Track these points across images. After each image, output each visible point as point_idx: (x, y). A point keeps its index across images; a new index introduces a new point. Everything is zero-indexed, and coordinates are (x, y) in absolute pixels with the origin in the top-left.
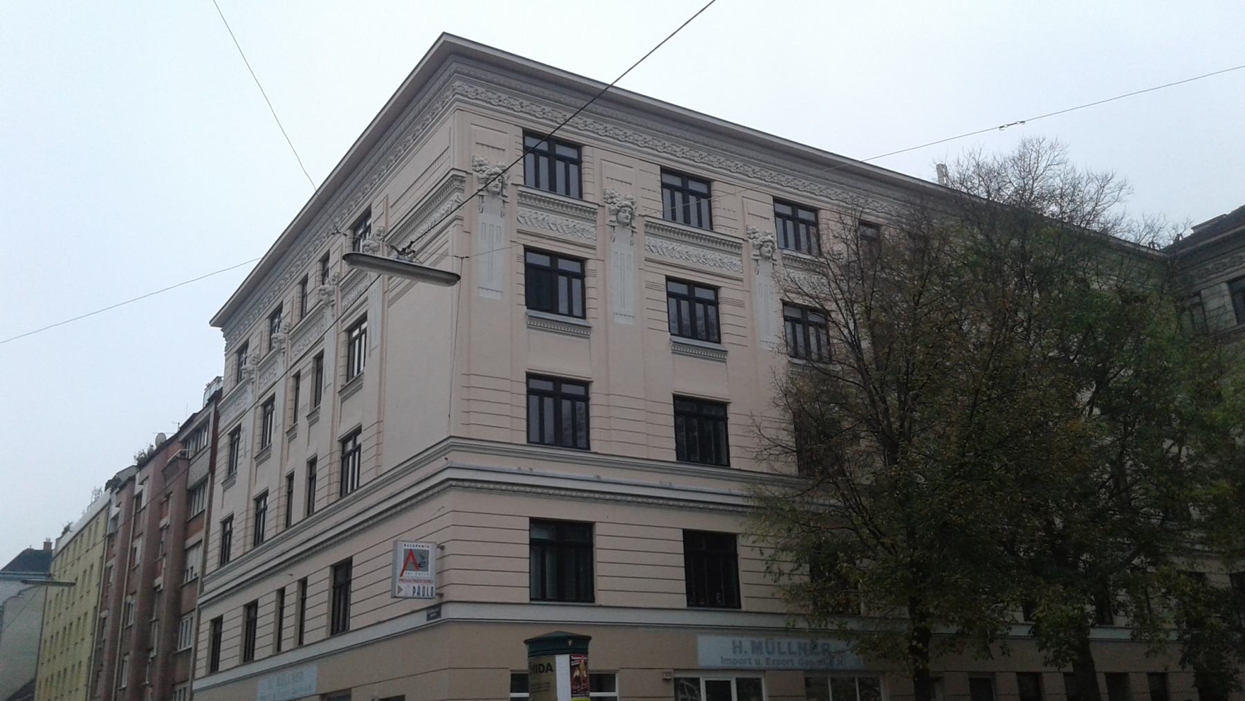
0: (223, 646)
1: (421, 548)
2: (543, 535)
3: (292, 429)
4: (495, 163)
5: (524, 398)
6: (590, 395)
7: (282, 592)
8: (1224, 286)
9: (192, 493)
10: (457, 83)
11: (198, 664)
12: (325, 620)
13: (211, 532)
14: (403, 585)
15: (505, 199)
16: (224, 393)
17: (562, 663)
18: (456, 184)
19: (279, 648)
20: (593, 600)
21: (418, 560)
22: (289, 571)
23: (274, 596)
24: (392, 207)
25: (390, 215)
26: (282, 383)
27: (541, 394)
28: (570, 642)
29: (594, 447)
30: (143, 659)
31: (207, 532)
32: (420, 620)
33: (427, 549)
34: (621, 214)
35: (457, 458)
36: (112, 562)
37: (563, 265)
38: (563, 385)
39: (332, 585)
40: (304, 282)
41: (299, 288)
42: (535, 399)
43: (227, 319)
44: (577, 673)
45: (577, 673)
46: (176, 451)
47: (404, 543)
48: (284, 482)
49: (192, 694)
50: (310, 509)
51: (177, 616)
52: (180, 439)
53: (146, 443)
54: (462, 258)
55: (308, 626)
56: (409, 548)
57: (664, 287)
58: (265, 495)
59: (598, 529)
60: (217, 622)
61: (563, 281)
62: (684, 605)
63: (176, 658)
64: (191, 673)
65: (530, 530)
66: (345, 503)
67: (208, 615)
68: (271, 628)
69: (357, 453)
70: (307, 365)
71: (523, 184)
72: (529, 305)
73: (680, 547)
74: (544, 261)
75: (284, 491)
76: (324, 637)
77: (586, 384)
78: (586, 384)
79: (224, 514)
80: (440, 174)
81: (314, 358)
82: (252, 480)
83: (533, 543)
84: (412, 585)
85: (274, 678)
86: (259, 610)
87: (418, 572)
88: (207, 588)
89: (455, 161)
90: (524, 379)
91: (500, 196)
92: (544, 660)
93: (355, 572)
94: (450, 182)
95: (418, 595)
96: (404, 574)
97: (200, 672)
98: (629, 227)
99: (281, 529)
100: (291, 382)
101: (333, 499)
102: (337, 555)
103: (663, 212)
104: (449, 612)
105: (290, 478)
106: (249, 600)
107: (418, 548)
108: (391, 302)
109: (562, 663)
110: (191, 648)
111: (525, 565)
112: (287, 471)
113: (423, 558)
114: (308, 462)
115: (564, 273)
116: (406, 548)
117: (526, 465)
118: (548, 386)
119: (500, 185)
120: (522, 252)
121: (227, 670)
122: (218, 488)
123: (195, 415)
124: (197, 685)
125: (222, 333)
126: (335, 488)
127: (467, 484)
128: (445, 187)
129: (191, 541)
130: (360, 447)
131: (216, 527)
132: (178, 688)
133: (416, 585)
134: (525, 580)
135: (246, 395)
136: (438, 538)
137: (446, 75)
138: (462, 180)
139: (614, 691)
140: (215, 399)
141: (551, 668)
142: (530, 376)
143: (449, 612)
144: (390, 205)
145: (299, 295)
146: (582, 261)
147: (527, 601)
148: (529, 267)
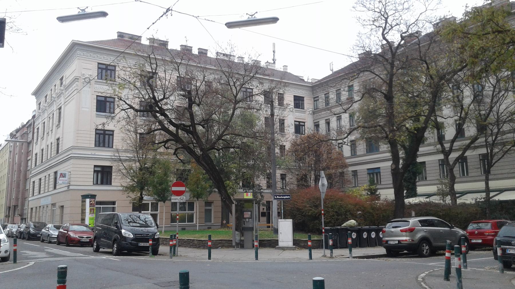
3: (43, 137)
4: (87, 73)
5: (94, 136)
7: (40, 179)
8: (323, 95)
9: (29, 143)
10: (78, 52)
14: (59, 181)
16: (36, 115)
17: (88, 201)
18: (76, 80)
19: (40, 193)
20: (111, 184)
21: (63, 175)
23: (38, 180)
26: (46, 119)
30: (18, 192)
31: (32, 157)
32: (66, 189)
35: (74, 151)
36: (11, 160)
42: (97, 136)
43: (37, 93)
44: (91, 203)
45: (91, 203)
46: (25, 130)
48: (41, 151)
49: (29, 201)
50: (36, 165)
51: (26, 179)
52: (27, 126)
53: (18, 126)
55: (35, 189)
60: (34, 182)
61: (108, 104)
63: (25, 190)
67: (32, 180)
70: (51, 116)
72: (97, 111)
75: (41, 153)
78: (113, 131)
80: (73, 77)
82: (41, 145)
85: (43, 199)
88: (32, 172)
89: (76, 74)
92: (84, 200)
94: (74, 80)
95: (63, 183)
97: (30, 196)
99: (46, 160)
100: (43, 124)
101: (55, 155)
102: (54, 170)
104: (71, 187)
108: (66, 105)
109: (88, 201)
112: (42, 148)
115: (108, 102)
117: (93, 152)
120: (96, 97)
122: (34, 144)
123: (29, 120)
124: (30, 199)
126: (56, 152)
128: (73, 81)
129: (29, 158)
131: (34, 155)
132: (26, 199)
135: (61, 98)
136: (69, 170)
137: (75, 49)
138: (78, 79)
139: (149, 204)
140: (34, 117)
141: (85, 202)
143: (71, 187)
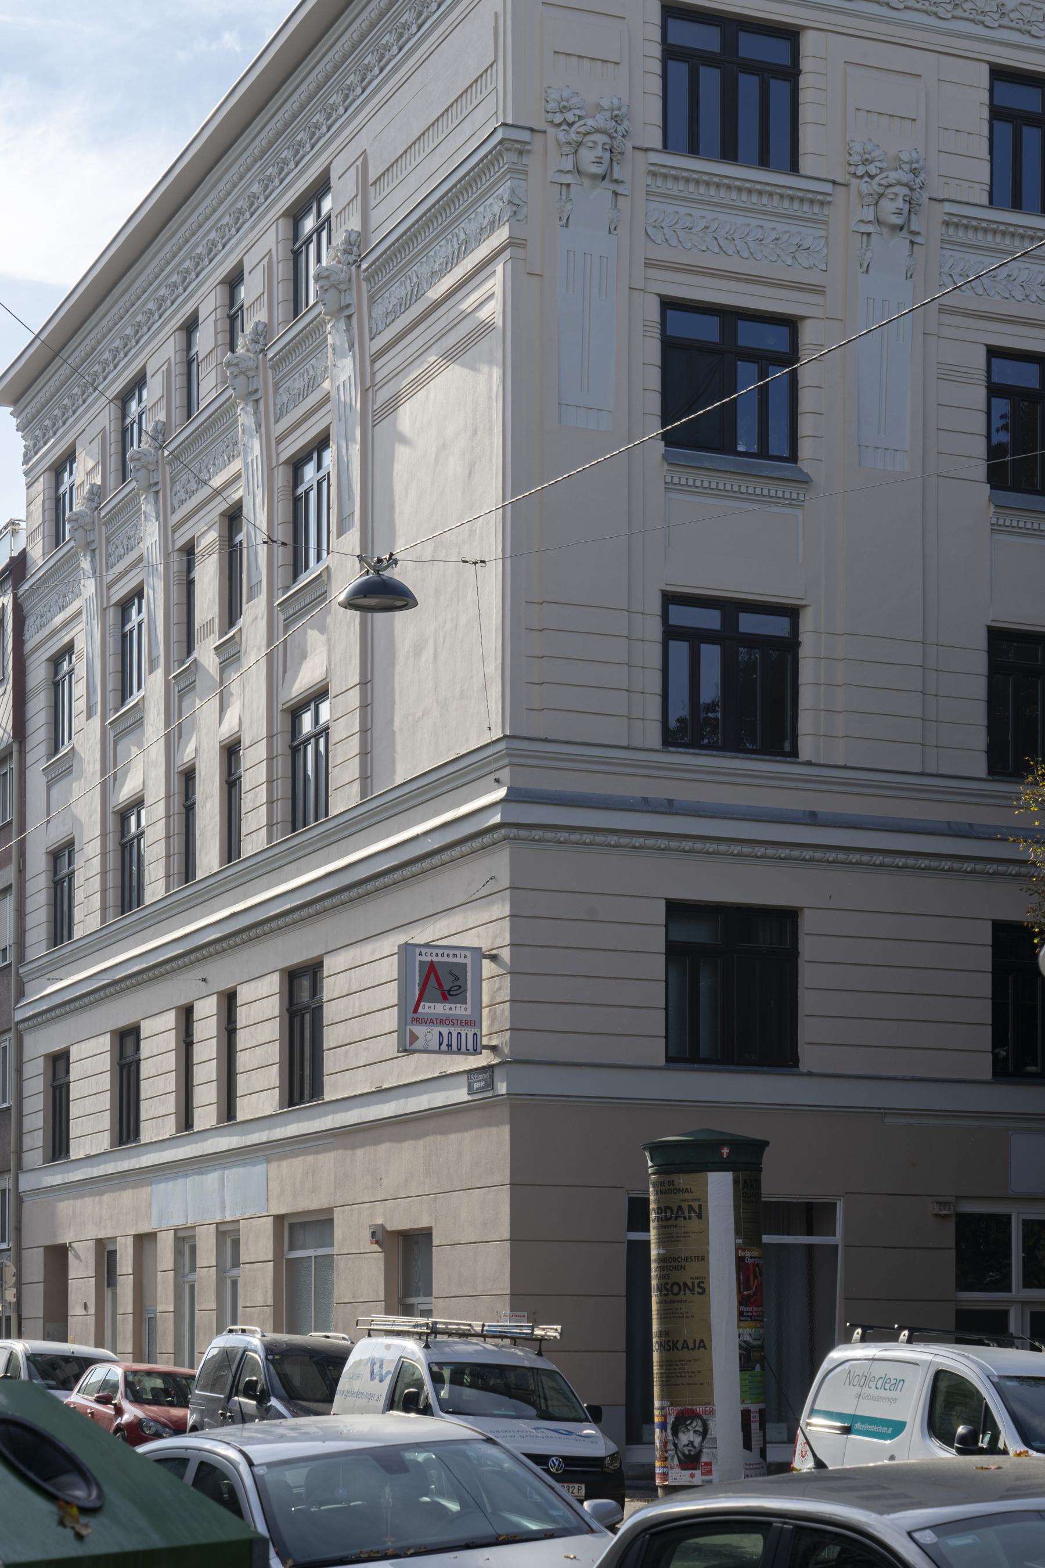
0: (75, 1110)
1: (451, 960)
2: (697, 934)
5: (657, 649)
6: (802, 638)
11: (28, 1142)
12: (273, 1076)
13: (30, 872)
15: (620, 189)
18: (509, 158)
22: (198, 973)
24: (375, 183)
25: (373, 203)
27: (695, 637)
28: (725, 1151)
29: (806, 748)
33: (462, 960)
34: (884, 203)
37: (748, 336)
38: (743, 616)
39: (286, 1005)
40: (190, 326)
41: (178, 339)
42: (680, 649)
47: (418, 951)
54: (475, 563)
55: (242, 1084)
56: (428, 959)
57: (981, 375)
58: (137, 803)
59: (807, 924)
60: (59, 1062)
62: (988, 1075)
64: (13, 1158)
65: (666, 926)
66: (301, 846)
68: (170, 1083)
69: (322, 741)
71: (660, 146)
73: (984, 959)
74: (708, 330)
76: (271, 1112)
77: (792, 612)
78: (792, 612)
79: (56, 836)
81: (222, 514)
83: (674, 951)
84: (436, 1030)
86: (143, 1044)
87: (448, 1006)
90: (655, 606)
91: (606, 183)
93: (331, 987)
96: (420, 1010)
98: (904, 232)
103: (991, 186)
105: (189, 776)
106: (123, 1021)
107: (445, 959)
110: (9, 1109)
111: (657, 994)
113: (457, 978)
114: (222, 748)
116: (424, 958)
118: (711, 620)
119: (608, 155)
121: (89, 1157)
125: (14, 421)
127: (537, 834)
130: (326, 731)
131: (38, 863)
133: (445, 1031)
134: (657, 1023)
142: (670, 599)
144: (371, 182)
145: (180, 357)
146: (790, 324)
147: (662, 1061)
148: (670, 346)
